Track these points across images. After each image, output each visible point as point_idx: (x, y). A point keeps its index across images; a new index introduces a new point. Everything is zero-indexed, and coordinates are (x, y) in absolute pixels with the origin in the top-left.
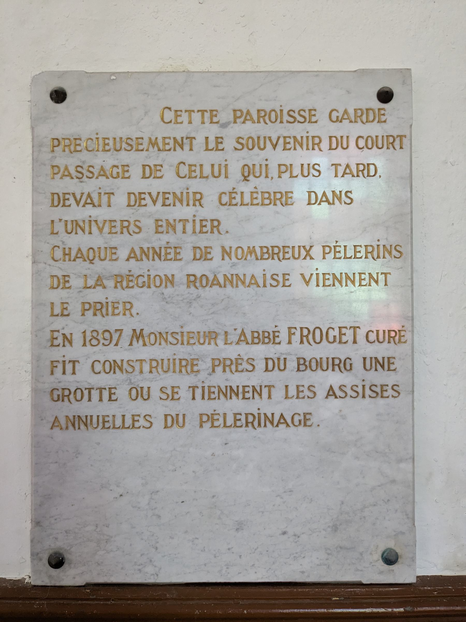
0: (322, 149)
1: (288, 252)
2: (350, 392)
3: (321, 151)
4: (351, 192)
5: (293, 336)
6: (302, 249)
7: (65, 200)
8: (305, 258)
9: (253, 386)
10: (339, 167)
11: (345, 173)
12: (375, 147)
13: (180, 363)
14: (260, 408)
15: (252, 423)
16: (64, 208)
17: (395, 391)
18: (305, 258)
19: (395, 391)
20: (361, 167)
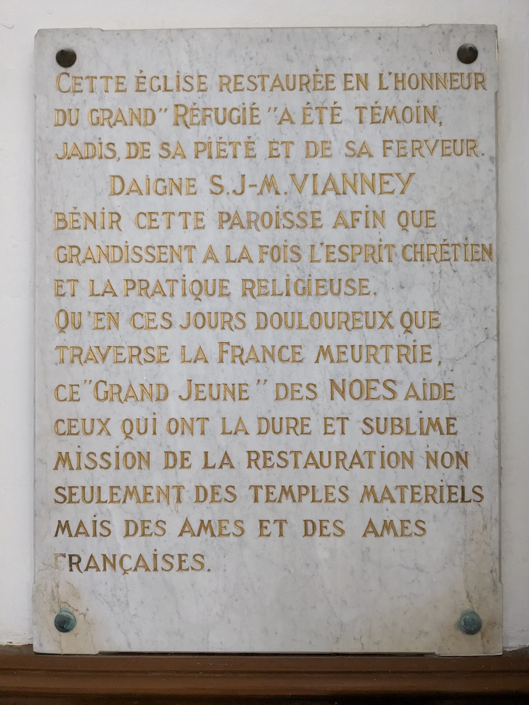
0: (424, 155)
1: (455, 494)
2: (100, 462)
3: (423, 157)
4: (220, 177)
5: (183, 563)
6: (378, 315)
7: (293, 391)
8: (100, 433)
9: (358, 75)
10: (299, 456)
11: (274, 86)
12: (228, 122)
13: (337, 457)
14: (367, 204)
15: (294, 428)
16: (393, 436)
17: (389, 389)
18: (100, 433)
19: (389, 389)
20: (253, 217)
